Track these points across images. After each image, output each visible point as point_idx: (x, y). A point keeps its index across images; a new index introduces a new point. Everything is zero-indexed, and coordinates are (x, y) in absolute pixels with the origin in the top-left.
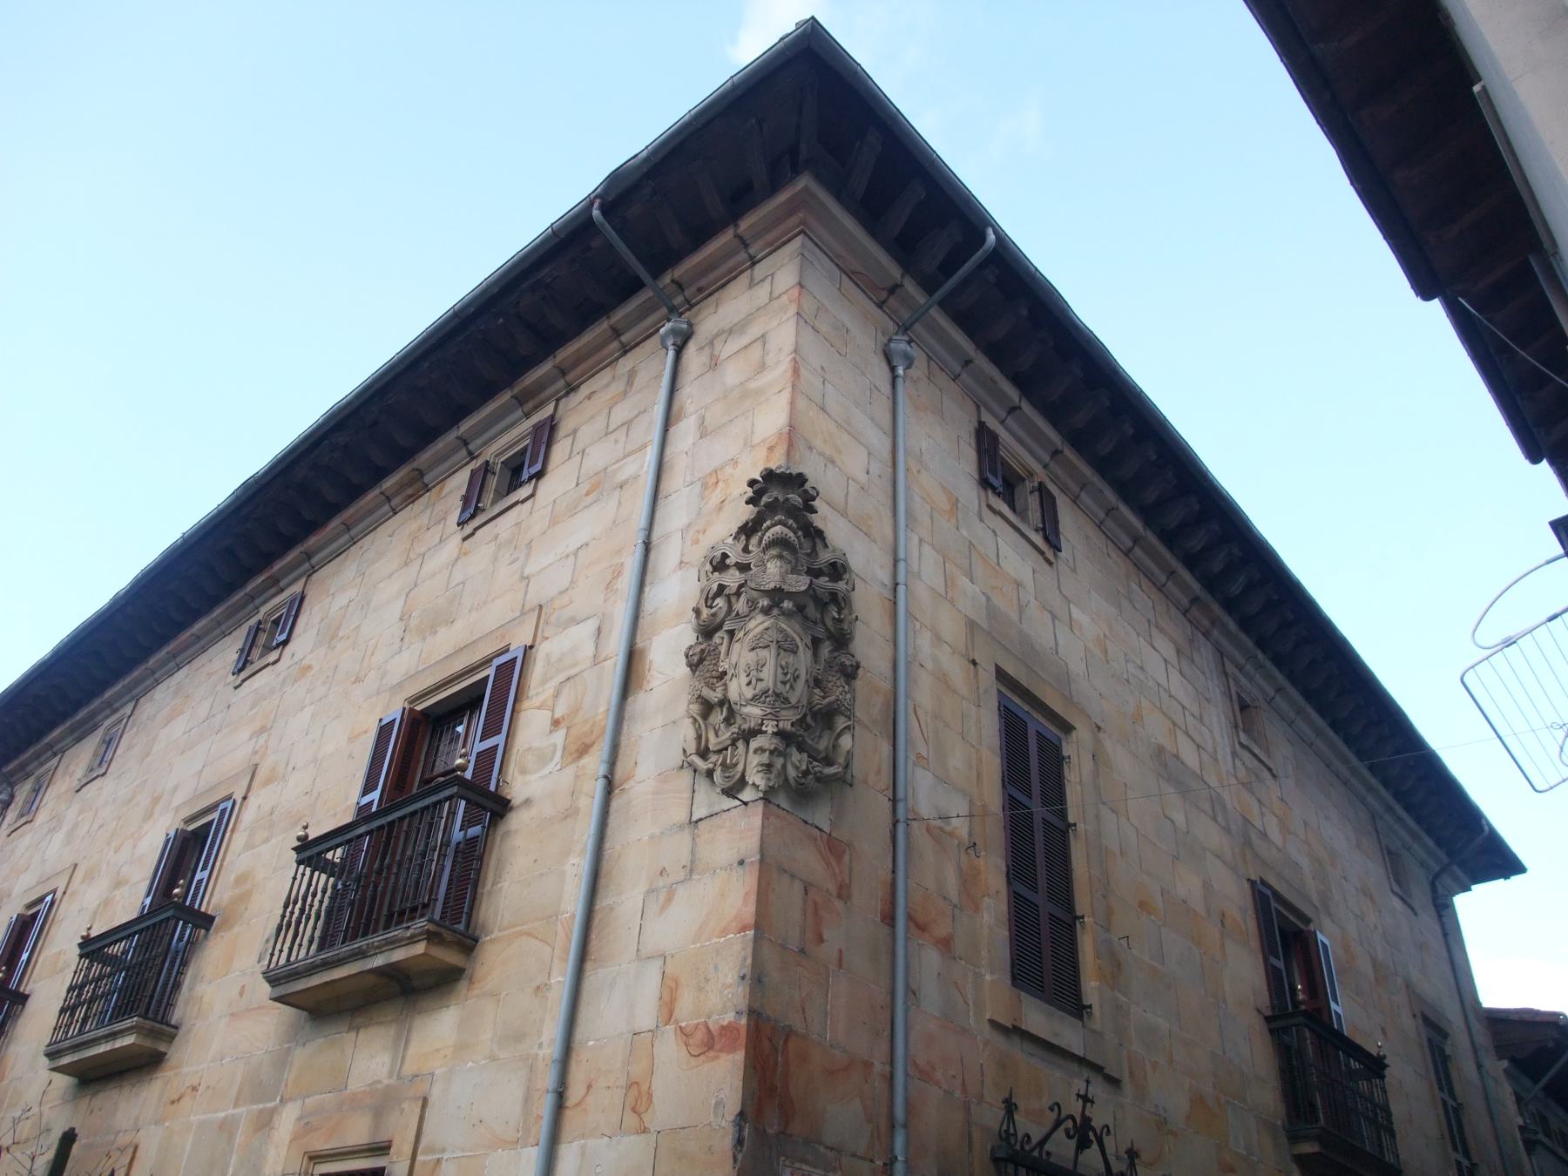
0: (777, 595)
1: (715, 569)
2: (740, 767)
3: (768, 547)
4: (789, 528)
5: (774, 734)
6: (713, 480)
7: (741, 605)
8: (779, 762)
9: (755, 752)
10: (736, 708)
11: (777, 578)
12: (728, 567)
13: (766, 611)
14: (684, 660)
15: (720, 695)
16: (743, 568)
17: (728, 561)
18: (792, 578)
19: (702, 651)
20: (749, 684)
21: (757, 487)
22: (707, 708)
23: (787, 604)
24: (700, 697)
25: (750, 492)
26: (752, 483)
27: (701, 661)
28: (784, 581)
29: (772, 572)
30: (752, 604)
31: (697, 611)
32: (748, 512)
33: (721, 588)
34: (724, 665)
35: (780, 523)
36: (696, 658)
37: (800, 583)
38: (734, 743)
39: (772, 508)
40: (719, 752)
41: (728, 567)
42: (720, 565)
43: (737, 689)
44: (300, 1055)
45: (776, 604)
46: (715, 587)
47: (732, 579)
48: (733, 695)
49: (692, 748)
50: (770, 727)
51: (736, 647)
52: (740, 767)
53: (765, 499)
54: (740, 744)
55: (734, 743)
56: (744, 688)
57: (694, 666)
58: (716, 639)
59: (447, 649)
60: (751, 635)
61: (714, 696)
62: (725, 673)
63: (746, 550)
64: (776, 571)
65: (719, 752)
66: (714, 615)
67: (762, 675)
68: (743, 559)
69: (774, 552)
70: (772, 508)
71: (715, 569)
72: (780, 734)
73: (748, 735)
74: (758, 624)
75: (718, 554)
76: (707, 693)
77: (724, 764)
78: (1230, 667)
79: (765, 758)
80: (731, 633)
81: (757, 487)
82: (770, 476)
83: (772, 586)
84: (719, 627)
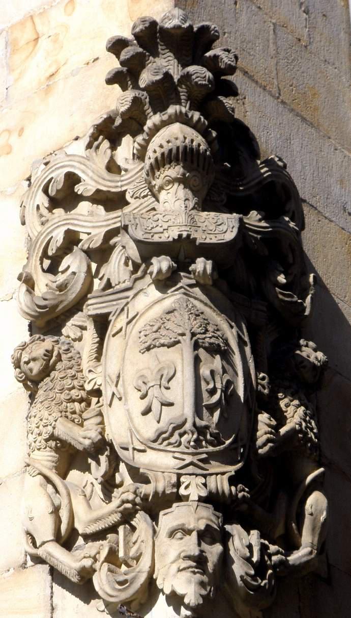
0: (182, 251)
1: (54, 203)
2: (145, 564)
3: (158, 165)
4: (195, 126)
5: (201, 499)
6: (29, 35)
7: (116, 269)
8: (214, 551)
9: (172, 534)
10: (121, 453)
11: (182, 219)
12: (80, 198)
13: (165, 283)
14: (12, 372)
15: (94, 435)
16: (112, 201)
17: (79, 189)
18: (208, 218)
19: (49, 354)
20: (147, 411)
21: (126, 54)
22: (70, 458)
23: (201, 265)
24: (52, 437)
25: (113, 64)
26: (117, 46)
27: (47, 371)
28: (193, 223)
29: (172, 210)
30: (138, 268)
31: (29, 282)
32: (118, 100)
33: (71, 240)
34: (95, 378)
35: (184, 119)
36: (36, 367)
37: (221, 227)
38: (127, 518)
39: (163, 93)
40: (99, 536)
41: (80, 198)
42: (65, 196)
43: (124, 422)
44: (162, 588)
45: (182, 264)
46: (59, 237)
47: (90, 221)
48: (117, 433)
49: (45, 532)
50: (194, 489)
51: (113, 344)
52: (145, 564)
53: (146, 77)
54: (141, 520)
55: (127, 518)
56: (139, 420)
57: (32, 384)
58: (69, 329)
59: (137, 325)
60: (140, 324)
61: (82, 436)
62: (97, 393)
63: (113, 167)
64: (180, 205)
65: (99, 536)
66: (62, 287)
67: (169, 396)
68: (111, 184)
69: (175, 171)
70: (163, 93)
71: (54, 203)
72: (212, 499)
73: (154, 506)
74: (150, 302)
75: (59, 176)
76: (64, 430)
77: (112, 557)
78: (27, 194)
79: (191, 545)
80: (102, 323)
81: (126, 54)
82: (151, 37)
83: (173, 234)
84: (77, 306)
